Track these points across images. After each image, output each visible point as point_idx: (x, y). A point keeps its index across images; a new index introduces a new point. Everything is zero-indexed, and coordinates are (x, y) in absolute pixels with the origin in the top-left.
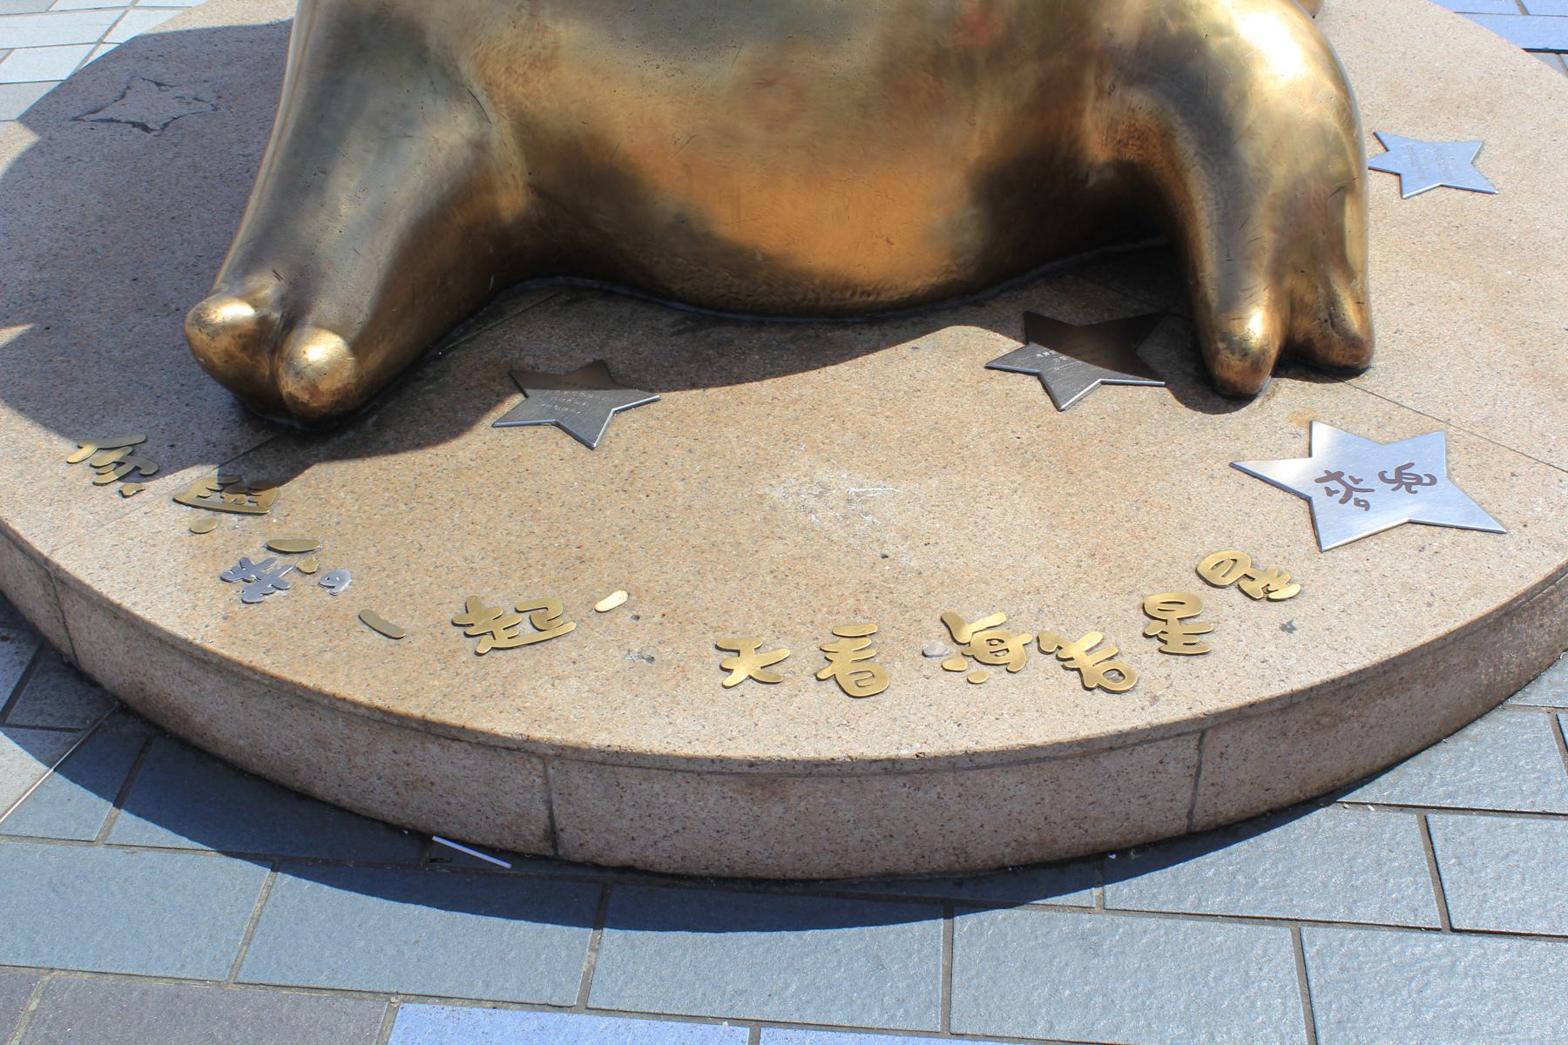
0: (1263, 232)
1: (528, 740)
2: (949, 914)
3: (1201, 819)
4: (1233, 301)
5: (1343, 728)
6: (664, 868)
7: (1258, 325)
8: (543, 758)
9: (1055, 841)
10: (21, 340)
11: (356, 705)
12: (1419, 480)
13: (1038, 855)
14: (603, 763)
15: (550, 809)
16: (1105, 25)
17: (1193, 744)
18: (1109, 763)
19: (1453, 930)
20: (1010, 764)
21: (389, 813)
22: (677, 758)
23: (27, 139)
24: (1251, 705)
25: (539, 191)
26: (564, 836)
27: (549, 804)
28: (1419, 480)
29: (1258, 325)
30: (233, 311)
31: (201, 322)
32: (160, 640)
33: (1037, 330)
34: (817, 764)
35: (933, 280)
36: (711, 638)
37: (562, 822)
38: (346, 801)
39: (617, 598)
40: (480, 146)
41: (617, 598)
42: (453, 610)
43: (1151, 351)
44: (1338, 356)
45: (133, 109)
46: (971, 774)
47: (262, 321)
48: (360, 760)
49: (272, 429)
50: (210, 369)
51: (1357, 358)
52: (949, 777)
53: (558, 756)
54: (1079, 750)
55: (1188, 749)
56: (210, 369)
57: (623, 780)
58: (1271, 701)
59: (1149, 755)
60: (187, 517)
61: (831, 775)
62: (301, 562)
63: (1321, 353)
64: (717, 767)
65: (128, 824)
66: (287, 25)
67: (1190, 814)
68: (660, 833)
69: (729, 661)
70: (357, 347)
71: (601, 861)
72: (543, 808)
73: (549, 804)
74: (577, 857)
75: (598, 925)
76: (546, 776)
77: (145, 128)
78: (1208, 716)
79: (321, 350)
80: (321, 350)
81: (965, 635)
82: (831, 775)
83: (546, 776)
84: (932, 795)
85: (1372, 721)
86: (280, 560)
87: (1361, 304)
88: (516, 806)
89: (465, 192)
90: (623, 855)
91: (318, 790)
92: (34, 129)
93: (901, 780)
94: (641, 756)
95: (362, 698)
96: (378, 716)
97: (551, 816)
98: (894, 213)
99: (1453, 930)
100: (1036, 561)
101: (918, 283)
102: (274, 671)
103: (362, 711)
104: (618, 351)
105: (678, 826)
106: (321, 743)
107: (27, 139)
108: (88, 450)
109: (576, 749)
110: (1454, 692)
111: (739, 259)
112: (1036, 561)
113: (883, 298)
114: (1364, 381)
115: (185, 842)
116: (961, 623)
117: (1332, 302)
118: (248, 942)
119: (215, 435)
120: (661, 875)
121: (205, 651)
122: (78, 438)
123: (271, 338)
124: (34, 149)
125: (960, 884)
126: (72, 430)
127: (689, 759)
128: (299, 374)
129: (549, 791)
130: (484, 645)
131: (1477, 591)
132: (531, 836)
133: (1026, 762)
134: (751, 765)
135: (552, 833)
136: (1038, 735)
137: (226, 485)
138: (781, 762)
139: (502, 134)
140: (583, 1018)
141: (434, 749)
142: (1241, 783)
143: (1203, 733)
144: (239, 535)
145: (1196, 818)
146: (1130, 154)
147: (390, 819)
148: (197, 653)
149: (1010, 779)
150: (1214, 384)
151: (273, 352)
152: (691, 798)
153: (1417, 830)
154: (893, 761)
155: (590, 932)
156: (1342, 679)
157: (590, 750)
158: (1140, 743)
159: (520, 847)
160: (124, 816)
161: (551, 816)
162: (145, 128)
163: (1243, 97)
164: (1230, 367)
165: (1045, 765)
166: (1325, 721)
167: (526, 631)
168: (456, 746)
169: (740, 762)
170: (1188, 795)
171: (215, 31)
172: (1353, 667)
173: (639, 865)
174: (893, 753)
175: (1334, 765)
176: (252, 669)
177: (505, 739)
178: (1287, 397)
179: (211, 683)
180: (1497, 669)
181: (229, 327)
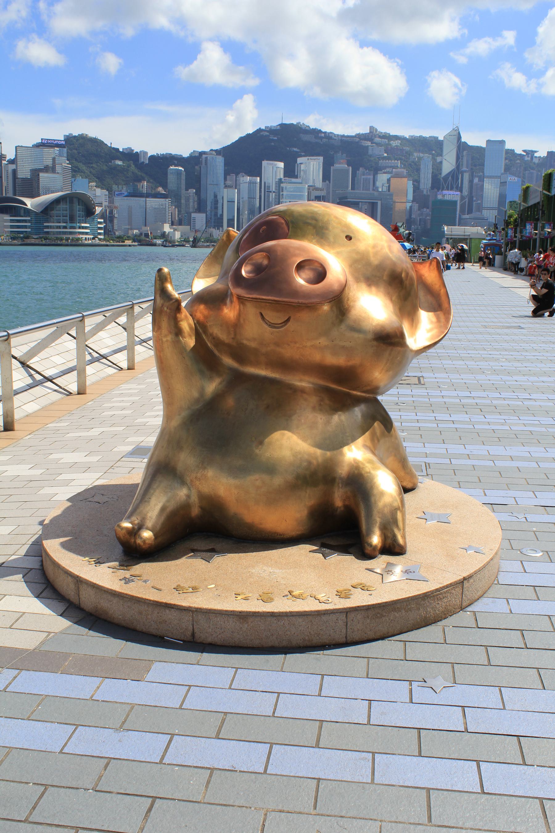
0: (378, 520)
1: (190, 607)
2: (286, 654)
3: (349, 639)
4: (370, 532)
5: (384, 619)
6: (219, 644)
7: (376, 540)
8: (193, 611)
9: (312, 640)
10: (70, 540)
11: (150, 600)
12: (411, 572)
13: (308, 644)
14: (206, 612)
15: (193, 627)
16: (340, 472)
17: (345, 616)
18: (324, 618)
19: (485, 793)
20: (300, 615)
21: (154, 632)
22: (223, 611)
23: (69, 504)
24: (358, 607)
25: (201, 507)
26: (196, 635)
27: (193, 625)
28: (411, 572)
29: (376, 540)
30: (127, 525)
31: (119, 526)
32: (104, 591)
33: (323, 545)
34: (255, 613)
35: (298, 533)
36: (234, 593)
37: (196, 630)
38: (144, 630)
39: (213, 586)
40: (188, 496)
41: (213, 586)
42: (175, 586)
43: (351, 550)
44: (397, 550)
45: (96, 499)
46: (291, 617)
47: (133, 528)
48: (149, 617)
49: (133, 553)
50: (119, 539)
51: (402, 550)
52: (286, 618)
53: (196, 611)
54: (316, 613)
55: (343, 617)
56: (119, 539)
57: (211, 617)
58: (363, 606)
59: (334, 617)
60: (111, 570)
61: (258, 616)
62: (138, 578)
63: (392, 548)
64: (232, 613)
65: (91, 633)
66: (137, 485)
67: (346, 637)
68: (218, 633)
69: (237, 596)
70: (156, 535)
71: (204, 642)
72: (191, 626)
73: (193, 625)
74: (199, 641)
75: (202, 652)
76: (193, 617)
77: (99, 503)
78: (348, 608)
79: (147, 534)
80: (147, 534)
81: (294, 594)
82: (258, 616)
83: (193, 617)
84: (282, 623)
85: (392, 618)
86: (133, 578)
87: (404, 537)
88: (185, 624)
89: (185, 507)
90: (209, 640)
91: (139, 628)
92: (70, 502)
93: (275, 618)
94: (215, 610)
95: (152, 599)
96: (155, 603)
97: (193, 629)
98: (289, 516)
99: (485, 793)
100: (314, 583)
101: (294, 533)
102: (132, 594)
103: (151, 602)
104: (218, 547)
105: (223, 631)
106: (140, 613)
107: (69, 504)
108: (87, 558)
109: (200, 609)
110: (414, 616)
111: (250, 526)
112: (314, 583)
113: (285, 537)
114: (404, 556)
115: (105, 636)
116: (293, 592)
117: (394, 536)
118: (120, 652)
119: (118, 557)
120: (218, 645)
121: (115, 591)
122: (85, 557)
123: (135, 532)
124: (70, 506)
125: (289, 649)
126: (84, 555)
127: (226, 611)
128: (141, 538)
129: (193, 621)
130: (181, 592)
131: (418, 590)
132: (189, 638)
133: (304, 615)
134: (240, 612)
135: (193, 634)
136: (307, 609)
137: (120, 565)
138: (247, 612)
139: (194, 499)
140: (198, 666)
141: (167, 611)
142: (358, 630)
143: (347, 613)
144: (123, 573)
145: (348, 638)
146: (347, 503)
147: (154, 633)
148: (113, 592)
149: (300, 620)
150: (364, 553)
151: (135, 535)
152: (226, 622)
153: (403, 646)
154: (273, 613)
155: (200, 654)
156: (381, 603)
157: (204, 609)
158: (331, 613)
159: (185, 639)
160: (91, 631)
161: (193, 629)
162: (99, 503)
163: (372, 487)
164: (368, 550)
165: (308, 617)
166: (378, 615)
167: (191, 590)
168: (173, 610)
169: (237, 612)
170: (345, 631)
171: (117, 485)
172: (384, 601)
173: (213, 643)
174: (273, 611)
175: (383, 629)
176: (126, 594)
177: (184, 607)
178: (383, 559)
179: (115, 600)
180: (426, 613)
181: (127, 528)
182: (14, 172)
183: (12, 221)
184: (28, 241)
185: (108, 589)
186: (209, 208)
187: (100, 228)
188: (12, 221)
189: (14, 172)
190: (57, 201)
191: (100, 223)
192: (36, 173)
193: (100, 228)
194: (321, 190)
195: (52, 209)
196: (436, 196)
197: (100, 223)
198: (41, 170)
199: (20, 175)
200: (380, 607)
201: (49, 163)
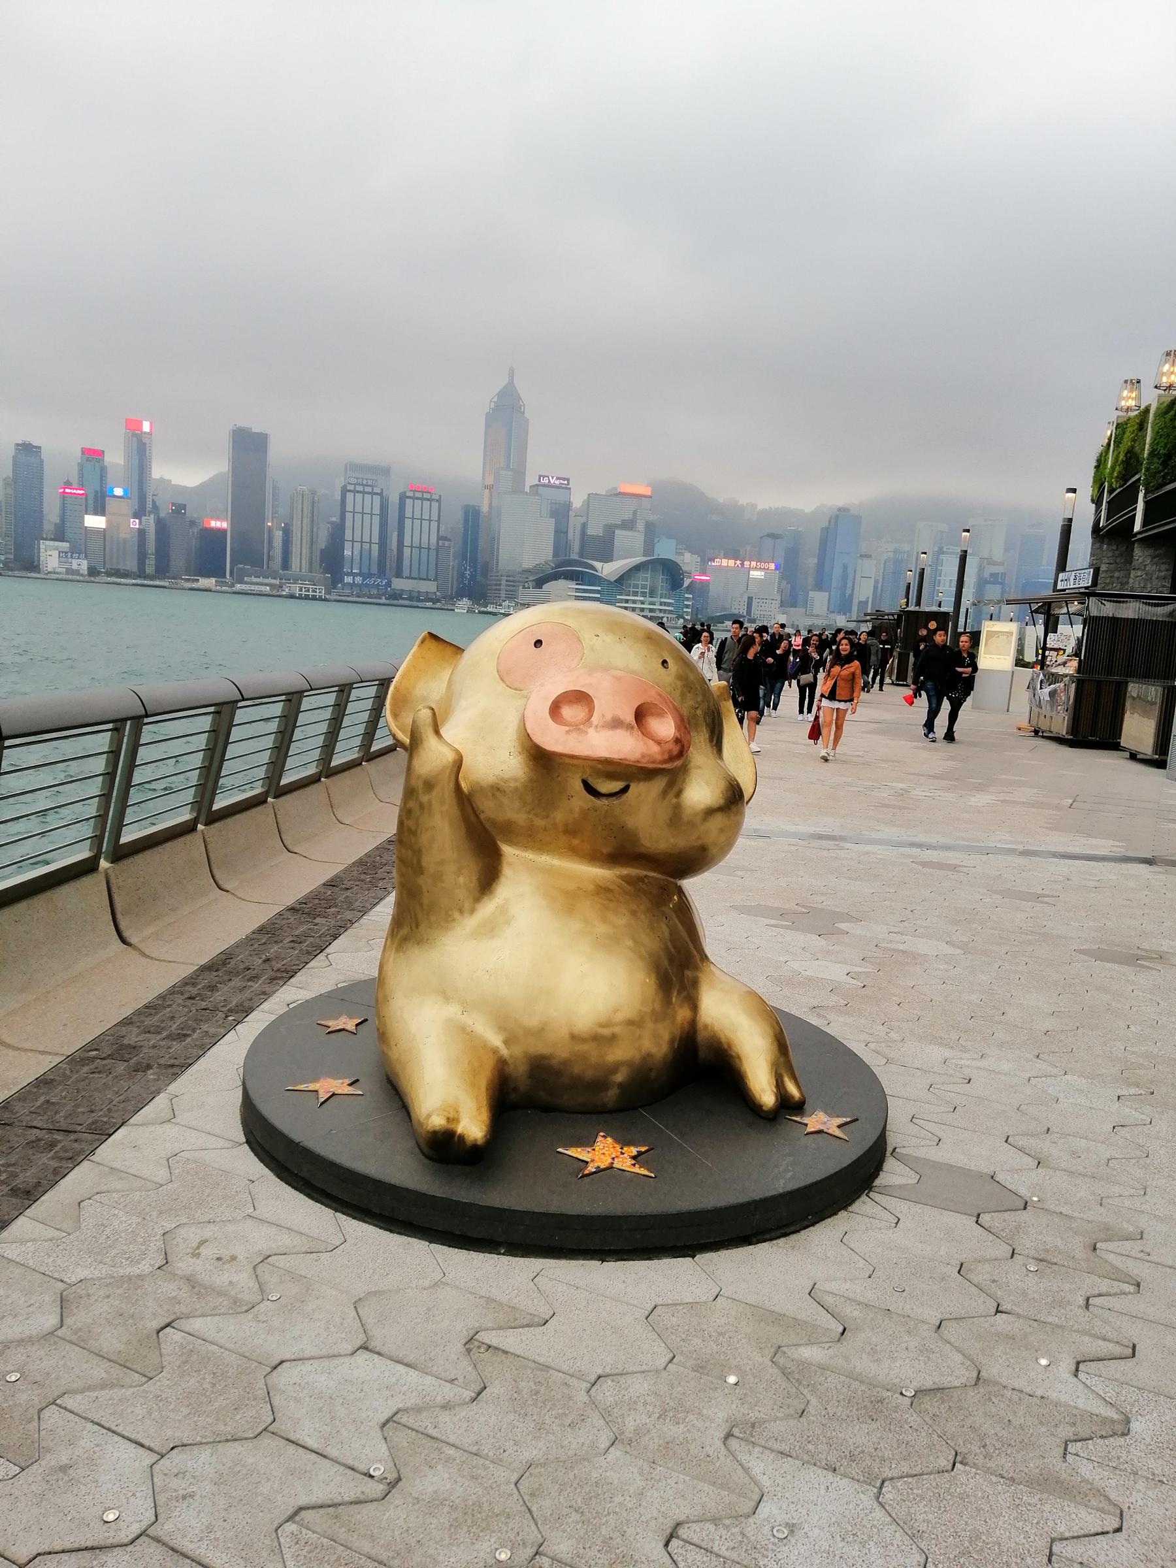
10: (566, 1146)
99: (361, 1347)
182: (584, 526)
183: (577, 590)
184: (438, 605)
185: (592, 1259)
186: (834, 584)
187: (687, 606)
188: (577, 590)
189: (584, 526)
190: (637, 568)
191: (688, 599)
192: (610, 530)
193: (687, 606)
194: (1002, 564)
195: (630, 578)
196: (140, 523)
197: (688, 599)
198: (617, 526)
199: (590, 532)
200: (763, 1232)
201: (628, 516)
